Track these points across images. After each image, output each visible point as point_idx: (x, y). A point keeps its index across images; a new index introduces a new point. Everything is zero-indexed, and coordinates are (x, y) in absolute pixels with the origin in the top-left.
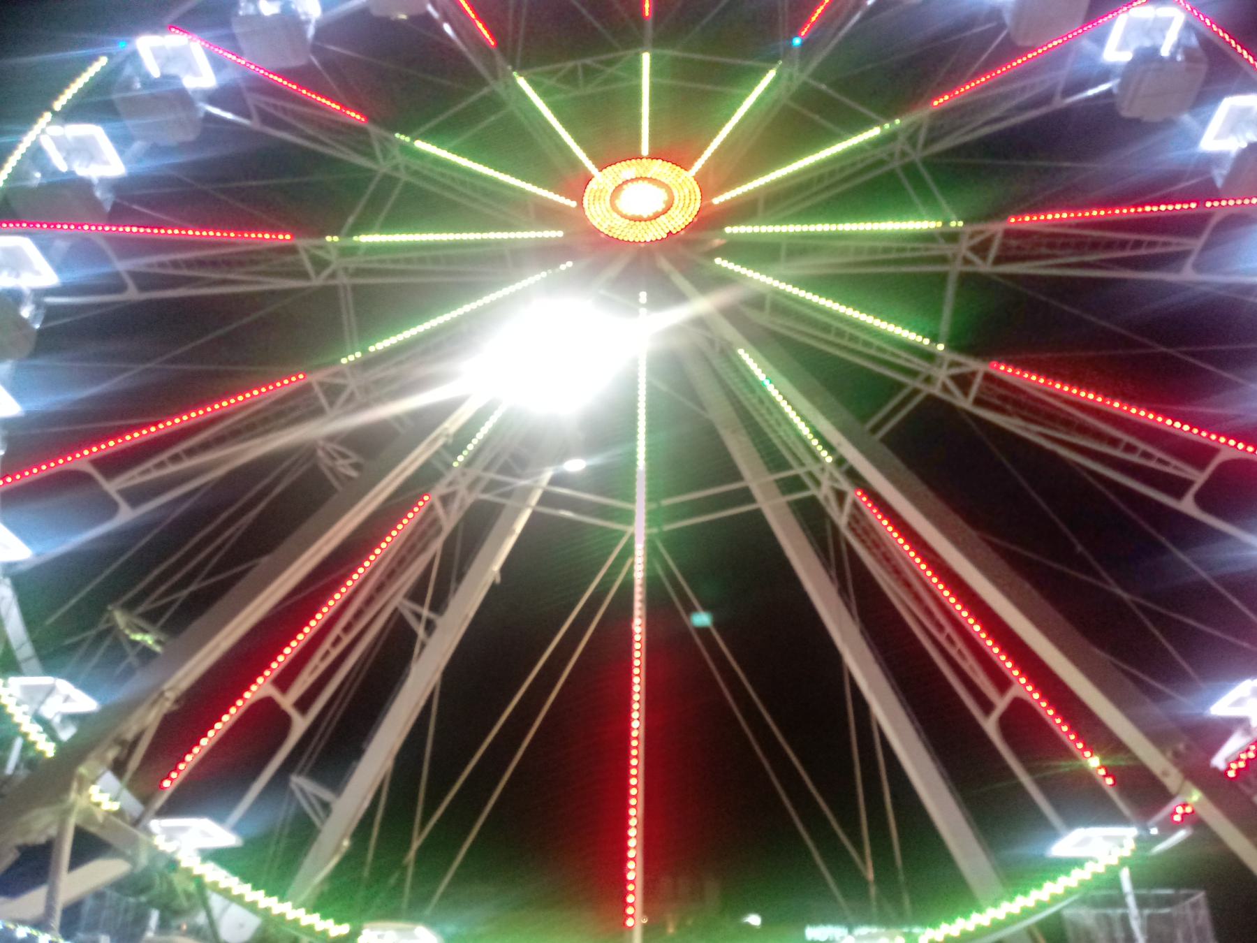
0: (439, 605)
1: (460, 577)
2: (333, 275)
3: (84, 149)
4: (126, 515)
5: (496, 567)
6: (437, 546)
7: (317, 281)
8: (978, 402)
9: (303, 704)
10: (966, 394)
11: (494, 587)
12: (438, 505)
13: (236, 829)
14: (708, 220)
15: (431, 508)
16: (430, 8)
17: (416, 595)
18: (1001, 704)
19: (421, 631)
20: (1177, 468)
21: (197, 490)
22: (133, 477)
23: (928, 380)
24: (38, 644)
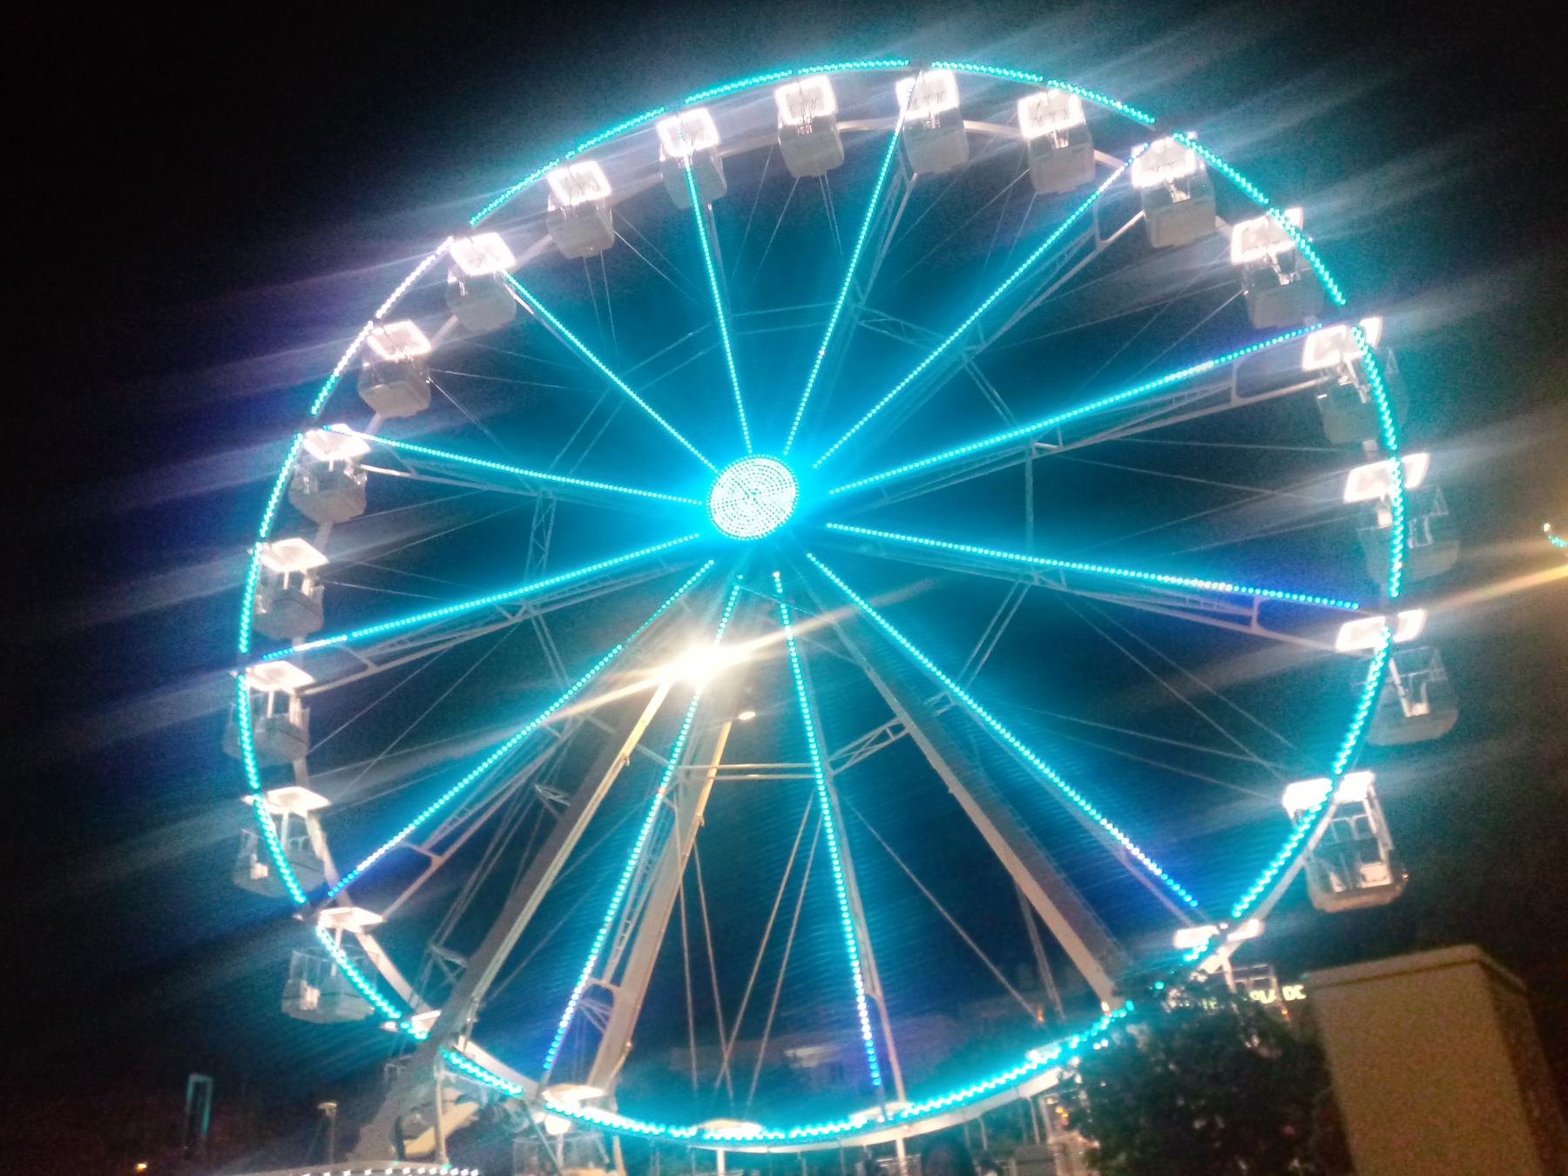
7: (518, 619)
11: (701, 829)
21: (435, 654)
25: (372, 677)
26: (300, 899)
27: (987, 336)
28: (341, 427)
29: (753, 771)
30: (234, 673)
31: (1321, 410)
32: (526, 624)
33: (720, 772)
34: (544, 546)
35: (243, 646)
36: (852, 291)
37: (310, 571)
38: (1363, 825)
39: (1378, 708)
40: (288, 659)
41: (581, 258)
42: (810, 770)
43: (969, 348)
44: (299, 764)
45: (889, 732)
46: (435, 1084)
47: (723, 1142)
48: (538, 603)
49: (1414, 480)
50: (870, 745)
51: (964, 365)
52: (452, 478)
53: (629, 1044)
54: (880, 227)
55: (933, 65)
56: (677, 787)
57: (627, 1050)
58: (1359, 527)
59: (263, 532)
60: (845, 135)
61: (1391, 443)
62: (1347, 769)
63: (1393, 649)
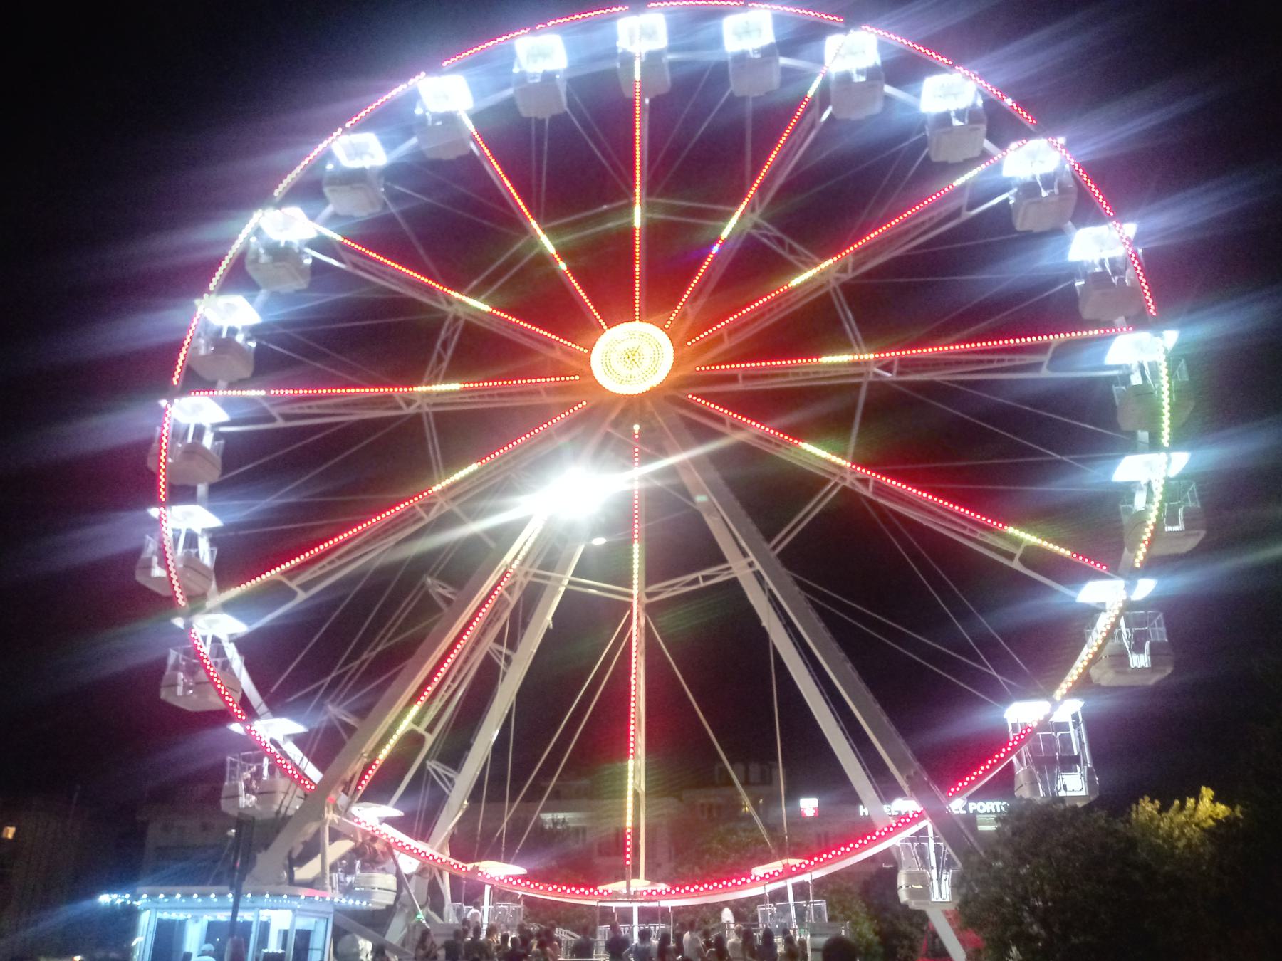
0: (512, 645)
1: (525, 625)
2: (419, 407)
4: (302, 596)
5: (549, 618)
6: (506, 615)
7: (411, 410)
9: (430, 729)
11: (548, 629)
12: (506, 594)
13: (396, 806)
15: (501, 595)
17: (499, 640)
19: (502, 664)
21: (337, 424)
22: (306, 576)
25: (278, 430)
27: (855, 267)
29: (594, 587)
30: (163, 403)
31: (1117, 401)
32: (417, 419)
33: (570, 583)
37: (244, 328)
38: (1066, 741)
39: (1103, 655)
40: (213, 397)
41: (530, 118)
43: (838, 275)
44: (202, 489)
45: (701, 579)
46: (324, 824)
48: (431, 402)
49: (1174, 471)
51: (829, 288)
53: (466, 802)
55: (863, 27)
57: (465, 807)
58: (1123, 503)
60: (673, 65)
61: (1165, 438)
62: (1065, 697)
63: (1129, 606)
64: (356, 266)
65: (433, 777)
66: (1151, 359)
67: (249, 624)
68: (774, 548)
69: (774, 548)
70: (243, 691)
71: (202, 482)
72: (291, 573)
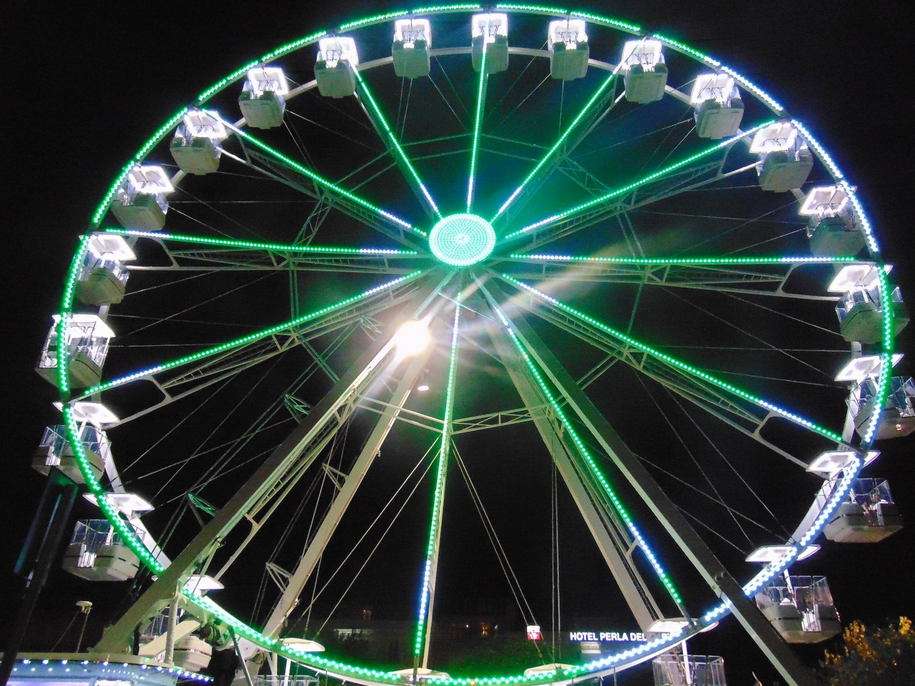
2: (287, 265)
3: (152, 179)
6: (335, 431)
7: (279, 268)
8: (644, 368)
10: (639, 363)
14: (502, 250)
16: (355, 93)
18: (632, 547)
20: (753, 419)
22: (174, 382)
23: (620, 353)
24: (123, 478)
26: (65, 388)
28: (215, 114)
32: (284, 274)
34: (314, 230)
35: (97, 219)
36: (562, 146)
42: (440, 426)
44: (105, 308)
46: (174, 602)
47: (293, 656)
50: (483, 423)
52: (272, 172)
54: (590, 117)
56: (346, 405)
57: (296, 604)
59: (138, 157)
64: (254, 161)
65: (270, 576)
66: (870, 288)
67: (121, 418)
68: (581, 385)
69: (581, 385)
70: (105, 472)
71: (105, 303)
72: (162, 377)
